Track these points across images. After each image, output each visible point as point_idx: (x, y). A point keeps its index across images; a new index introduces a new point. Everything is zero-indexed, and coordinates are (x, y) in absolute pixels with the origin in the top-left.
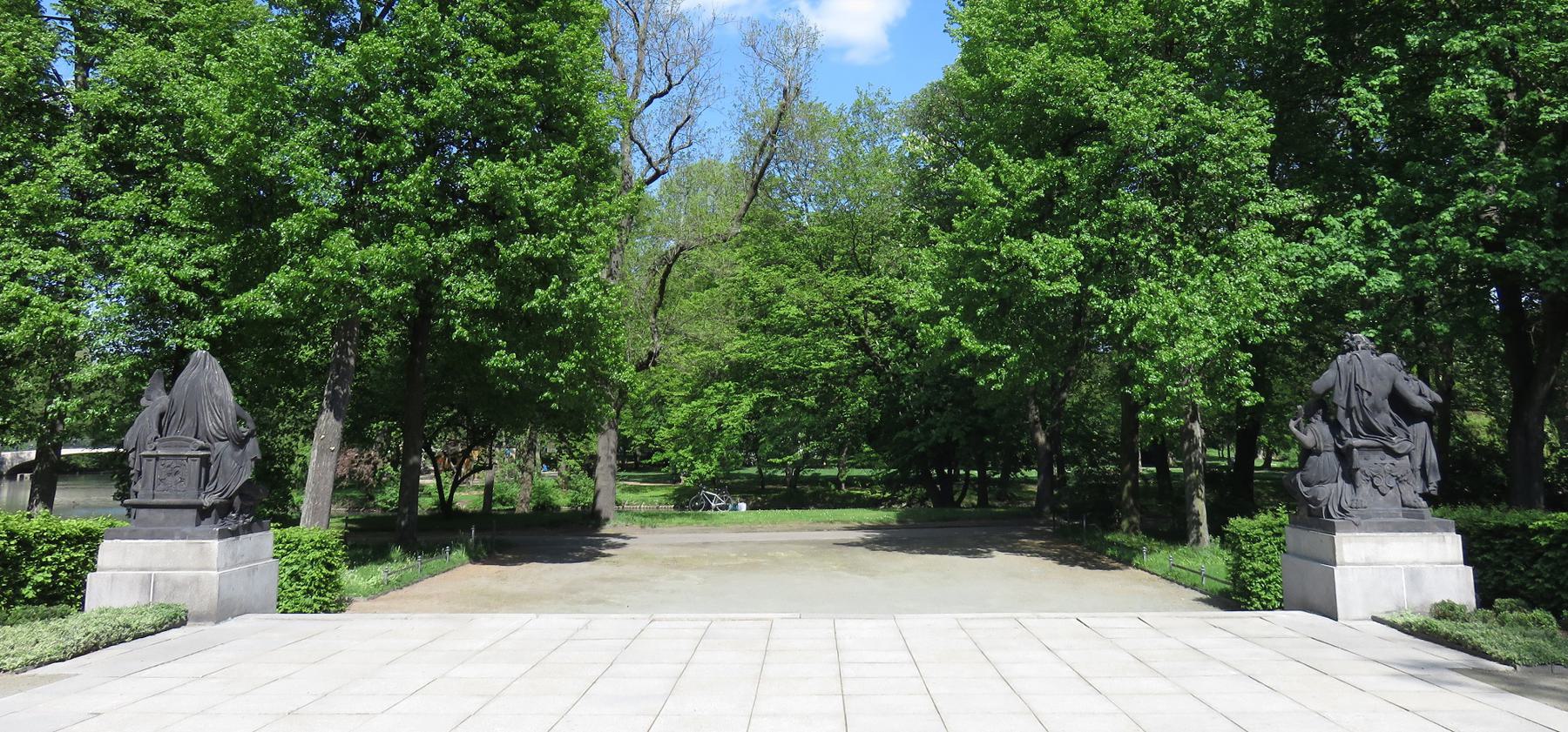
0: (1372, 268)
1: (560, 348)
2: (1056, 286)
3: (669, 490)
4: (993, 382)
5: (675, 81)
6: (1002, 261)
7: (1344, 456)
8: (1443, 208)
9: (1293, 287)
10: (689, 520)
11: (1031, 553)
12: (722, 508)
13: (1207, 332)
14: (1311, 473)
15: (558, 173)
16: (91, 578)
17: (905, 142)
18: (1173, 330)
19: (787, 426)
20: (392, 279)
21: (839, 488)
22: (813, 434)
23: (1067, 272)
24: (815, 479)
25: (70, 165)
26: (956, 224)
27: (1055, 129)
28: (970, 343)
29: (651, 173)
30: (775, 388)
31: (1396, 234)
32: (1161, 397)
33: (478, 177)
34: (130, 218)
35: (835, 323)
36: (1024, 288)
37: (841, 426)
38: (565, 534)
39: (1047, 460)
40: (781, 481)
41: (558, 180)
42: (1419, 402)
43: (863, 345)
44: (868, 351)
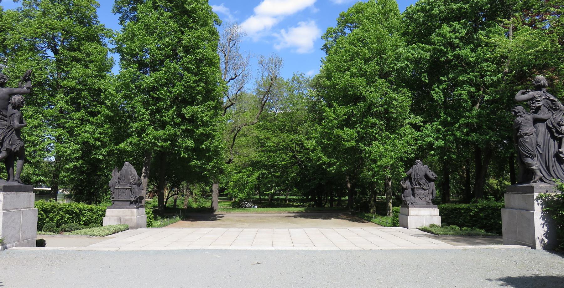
0: (437, 139)
1: (209, 159)
2: (349, 143)
3: (230, 202)
4: (331, 170)
5: (238, 75)
6: (335, 136)
7: (413, 190)
8: (456, 123)
9: (416, 144)
10: (241, 210)
11: (343, 219)
12: (250, 207)
13: (391, 157)
14: (405, 194)
15: (209, 109)
16: (105, 219)
17: (308, 92)
18: (381, 156)
19: (269, 182)
20: (165, 140)
21: (286, 202)
22: (278, 185)
23: (353, 139)
24: (278, 199)
25: (61, 104)
26: (323, 124)
27: (351, 98)
28: (325, 159)
29: (230, 103)
30: (266, 170)
31: (443, 130)
32: (378, 175)
33: (188, 111)
34: (79, 119)
35: (286, 149)
36: (340, 144)
37: (287, 182)
38: (205, 214)
39: (352, 193)
40: (267, 200)
41: (209, 111)
42: (432, 177)
43: (294, 156)
44: (296, 158)
